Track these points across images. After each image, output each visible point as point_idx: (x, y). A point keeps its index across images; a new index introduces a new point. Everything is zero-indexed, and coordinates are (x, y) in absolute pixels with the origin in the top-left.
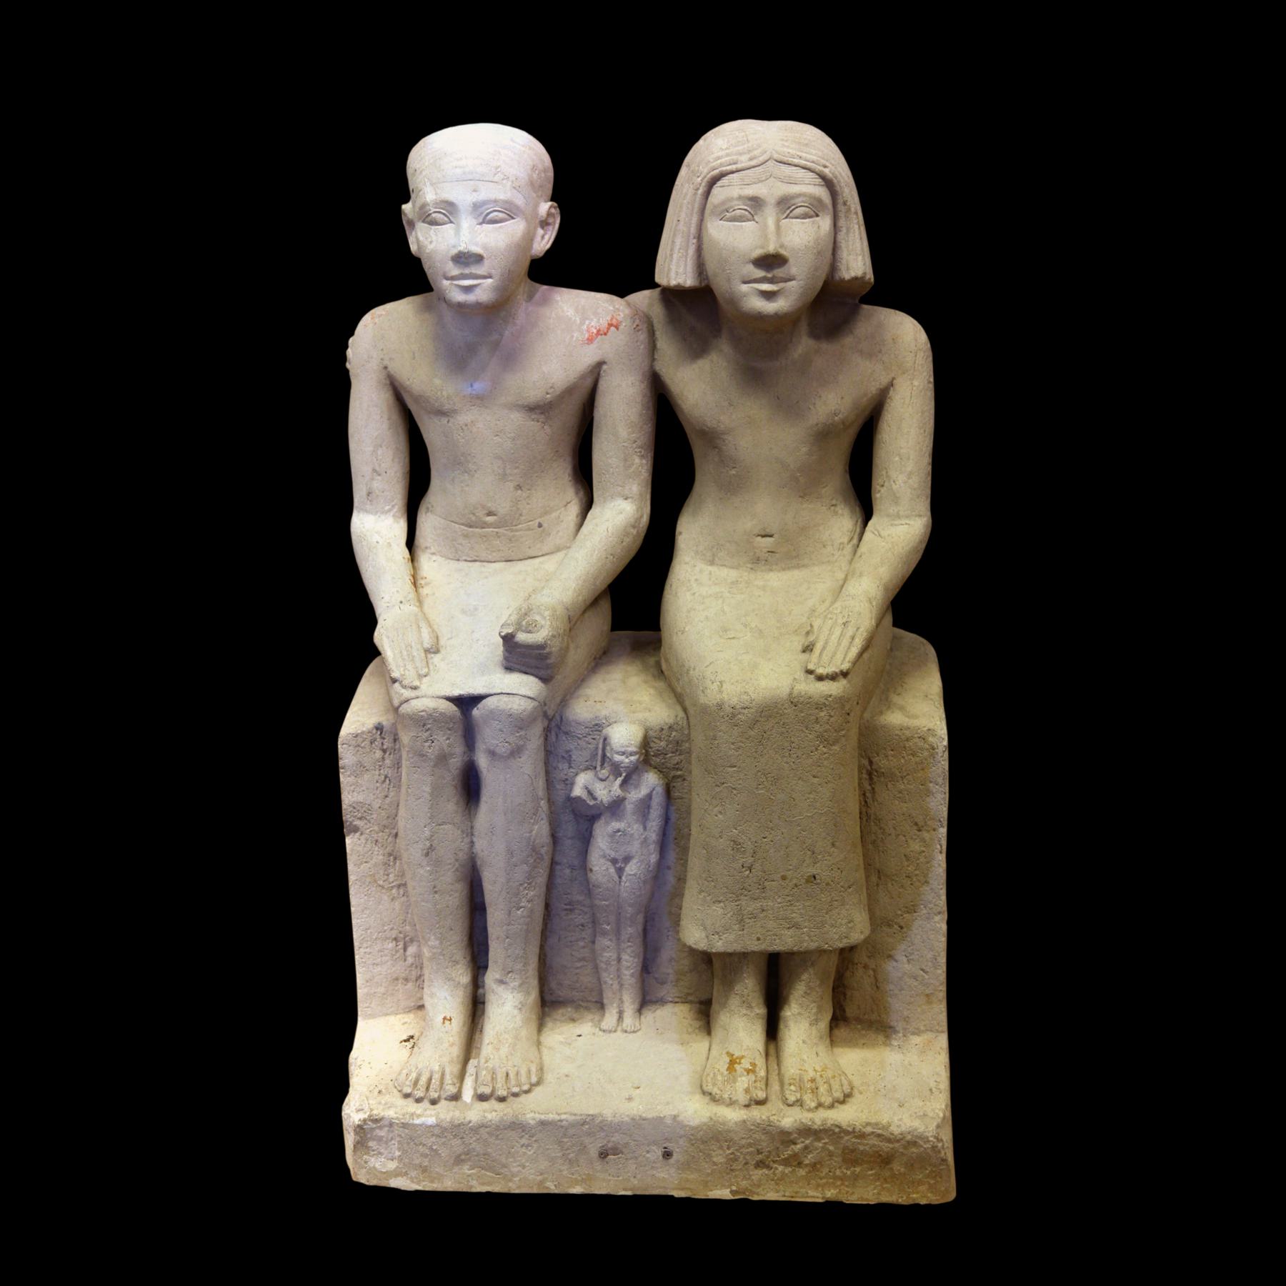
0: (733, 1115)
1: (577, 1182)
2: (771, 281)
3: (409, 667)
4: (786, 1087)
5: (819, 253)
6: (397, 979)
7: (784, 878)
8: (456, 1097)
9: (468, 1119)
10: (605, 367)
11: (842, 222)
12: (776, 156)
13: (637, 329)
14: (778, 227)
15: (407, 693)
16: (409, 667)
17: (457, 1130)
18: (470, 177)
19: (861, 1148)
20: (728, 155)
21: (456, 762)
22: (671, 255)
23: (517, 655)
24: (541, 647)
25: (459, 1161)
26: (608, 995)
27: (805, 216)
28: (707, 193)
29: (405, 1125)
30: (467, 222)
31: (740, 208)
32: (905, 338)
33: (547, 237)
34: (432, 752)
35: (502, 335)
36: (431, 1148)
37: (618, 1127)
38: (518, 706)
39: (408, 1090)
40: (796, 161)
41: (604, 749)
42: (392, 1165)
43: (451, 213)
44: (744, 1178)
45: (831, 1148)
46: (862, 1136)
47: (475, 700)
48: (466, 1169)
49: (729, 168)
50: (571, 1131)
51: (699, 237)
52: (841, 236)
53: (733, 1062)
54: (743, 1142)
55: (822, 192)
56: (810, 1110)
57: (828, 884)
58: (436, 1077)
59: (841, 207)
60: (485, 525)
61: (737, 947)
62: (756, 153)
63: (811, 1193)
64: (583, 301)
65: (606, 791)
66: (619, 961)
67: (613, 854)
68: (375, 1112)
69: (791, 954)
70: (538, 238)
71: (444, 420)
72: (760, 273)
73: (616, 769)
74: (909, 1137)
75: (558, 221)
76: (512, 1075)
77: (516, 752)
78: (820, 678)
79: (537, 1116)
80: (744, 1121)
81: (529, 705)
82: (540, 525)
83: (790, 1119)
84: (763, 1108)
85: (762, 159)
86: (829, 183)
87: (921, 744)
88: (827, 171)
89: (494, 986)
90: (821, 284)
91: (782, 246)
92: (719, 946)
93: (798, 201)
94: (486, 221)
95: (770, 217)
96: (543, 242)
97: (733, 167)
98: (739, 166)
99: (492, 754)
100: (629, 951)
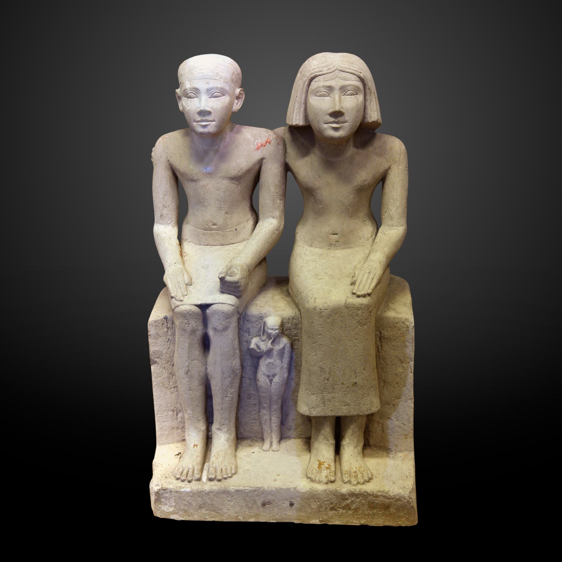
0: (320, 487)
1: (252, 517)
3: (179, 291)
4: (344, 475)
6: (173, 428)
7: (343, 384)
8: (199, 480)
9: (205, 489)
10: (264, 160)
12: (339, 68)
13: (278, 144)
14: (340, 99)
15: (178, 303)
16: (179, 291)
17: (200, 494)
18: (206, 77)
19: (376, 502)
20: (318, 68)
21: (199, 333)
22: (293, 112)
23: (226, 286)
24: (237, 283)
25: (200, 507)
26: (266, 435)
28: (309, 84)
29: (177, 492)
30: (204, 97)
32: (394, 150)
33: (239, 104)
34: (189, 329)
35: (219, 147)
36: (188, 502)
37: (270, 493)
38: (227, 308)
39: (178, 476)
40: (348, 70)
41: (264, 327)
42: (171, 509)
43: (197, 93)
44: (325, 515)
45: (363, 502)
46: (377, 496)
47: (208, 306)
48: (204, 511)
49: (318, 73)
50: (250, 494)
53: (320, 464)
54: (325, 499)
55: (359, 84)
56: (354, 485)
57: (362, 386)
58: (191, 471)
60: (212, 230)
61: (322, 414)
63: (354, 521)
64: (255, 132)
65: (265, 346)
66: (270, 420)
67: (268, 373)
68: (164, 486)
69: (346, 417)
70: (235, 104)
71: (194, 184)
72: (332, 119)
73: (269, 336)
74: (397, 497)
75: (244, 97)
76: (224, 470)
77: (225, 329)
78: (358, 296)
79: (235, 488)
80: (325, 490)
81: (231, 308)
82: (236, 230)
83: (345, 489)
84: (333, 484)
85: (333, 69)
86: (362, 80)
87: (402, 325)
89: (216, 431)
92: (314, 413)
93: (349, 88)
94: (213, 96)
96: (237, 106)
98: (323, 73)
99: (215, 329)
100: (275, 415)
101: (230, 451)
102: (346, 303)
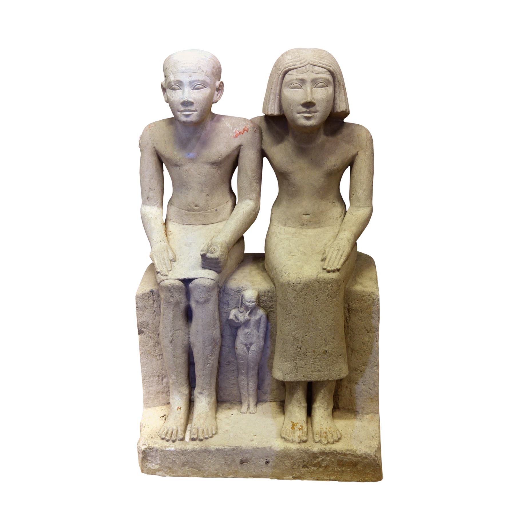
0: (293, 447)
2: (309, 112)
3: (164, 267)
4: (315, 435)
5: (328, 101)
6: (159, 392)
7: (314, 352)
8: (183, 439)
9: (187, 448)
10: (242, 147)
11: (337, 89)
12: (311, 62)
13: (255, 132)
14: (312, 91)
15: (163, 278)
16: (164, 267)
17: (183, 452)
18: (188, 71)
19: (345, 460)
20: (291, 62)
21: (183, 305)
22: (269, 102)
23: (207, 262)
24: (217, 259)
26: (243, 399)
27: (322, 87)
28: (283, 77)
29: (162, 451)
30: (187, 89)
31: (296, 83)
34: (173, 301)
35: (201, 134)
36: (172, 460)
38: (208, 283)
39: (163, 436)
40: (319, 64)
41: (242, 300)
43: (181, 85)
44: (298, 472)
45: (333, 460)
46: (345, 455)
47: (190, 280)
49: (292, 67)
50: (229, 453)
51: (280, 95)
52: (337, 95)
53: (293, 425)
54: (298, 457)
55: (329, 77)
56: (324, 445)
57: (331, 354)
58: (175, 431)
59: (337, 83)
60: (194, 210)
61: (295, 379)
62: (303, 61)
65: (242, 317)
66: (248, 385)
67: (245, 342)
68: (150, 445)
69: (317, 382)
70: (216, 95)
71: (178, 168)
72: (304, 109)
73: (247, 308)
74: (364, 455)
76: (205, 431)
77: (207, 301)
78: (329, 272)
79: (215, 447)
80: (298, 449)
81: (212, 282)
82: (216, 210)
83: (316, 448)
84: (305, 444)
85: (305, 64)
87: (369, 298)
88: (331, 68)
89: (198, 395)
90: (329, 114)
91: (313, 99)
92: (288, 379)
93: (320, 81)
94: (195, 88)
95: (308, 87)
97: (294, 67)
98: (296, 66)
99: (197, 302)
100: (252, 381)
101: (211, 413)
102: (317, 278)
